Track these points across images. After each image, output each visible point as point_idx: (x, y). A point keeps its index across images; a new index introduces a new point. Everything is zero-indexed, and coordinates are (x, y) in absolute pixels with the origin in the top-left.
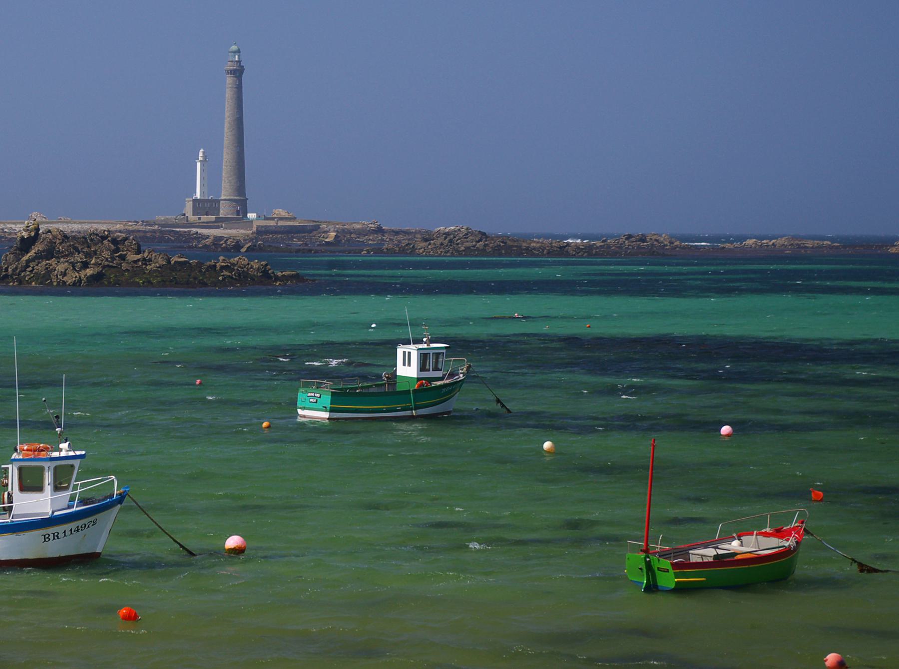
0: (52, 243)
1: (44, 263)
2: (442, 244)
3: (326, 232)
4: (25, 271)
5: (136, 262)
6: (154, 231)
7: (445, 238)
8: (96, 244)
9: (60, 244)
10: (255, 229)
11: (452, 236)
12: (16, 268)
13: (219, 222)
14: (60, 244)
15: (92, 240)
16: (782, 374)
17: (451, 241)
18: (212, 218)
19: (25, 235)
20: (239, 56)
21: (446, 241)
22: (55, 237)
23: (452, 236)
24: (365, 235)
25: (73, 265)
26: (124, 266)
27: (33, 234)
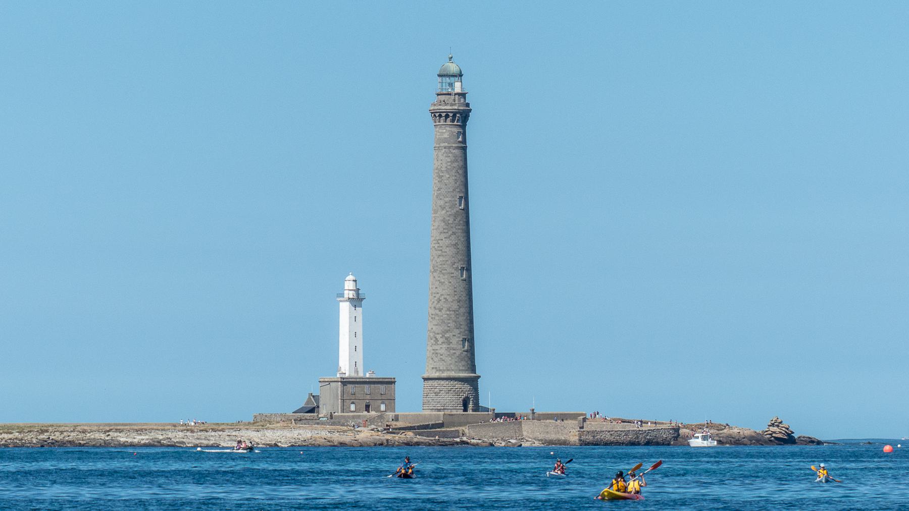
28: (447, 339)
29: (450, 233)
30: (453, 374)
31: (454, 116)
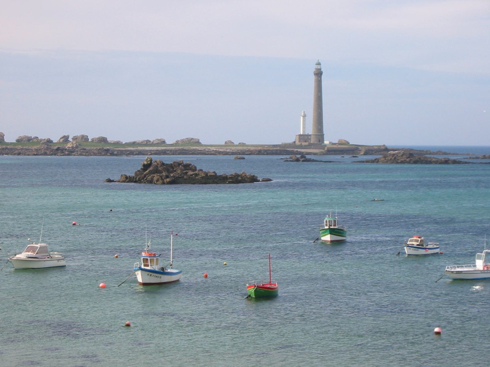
0: (157, 166)
1: (152, 176)
2: (391, 159)
3: (360, 150)
4: (143, 179)
5: (192, 175)
6: (277, 150)
7: (393, 156)
8: (176, 167)
9: (160, 167)
10: (326, 149)
11: (396, 156)
12: (140, 178)
13: (310, 146)
14: (160, 167)
15: (174, 165)
16: (138, 290)
17: (395, 158)
18: (307, 143)
19: (145, 163)
20: (320, 67)
21: (393, 158)
22: (158, 164)
23: (396, 156)
24: (379, 152)
25: (161, 177)
26: (185, 177)
27: (149, 162)
30: (317, 134)
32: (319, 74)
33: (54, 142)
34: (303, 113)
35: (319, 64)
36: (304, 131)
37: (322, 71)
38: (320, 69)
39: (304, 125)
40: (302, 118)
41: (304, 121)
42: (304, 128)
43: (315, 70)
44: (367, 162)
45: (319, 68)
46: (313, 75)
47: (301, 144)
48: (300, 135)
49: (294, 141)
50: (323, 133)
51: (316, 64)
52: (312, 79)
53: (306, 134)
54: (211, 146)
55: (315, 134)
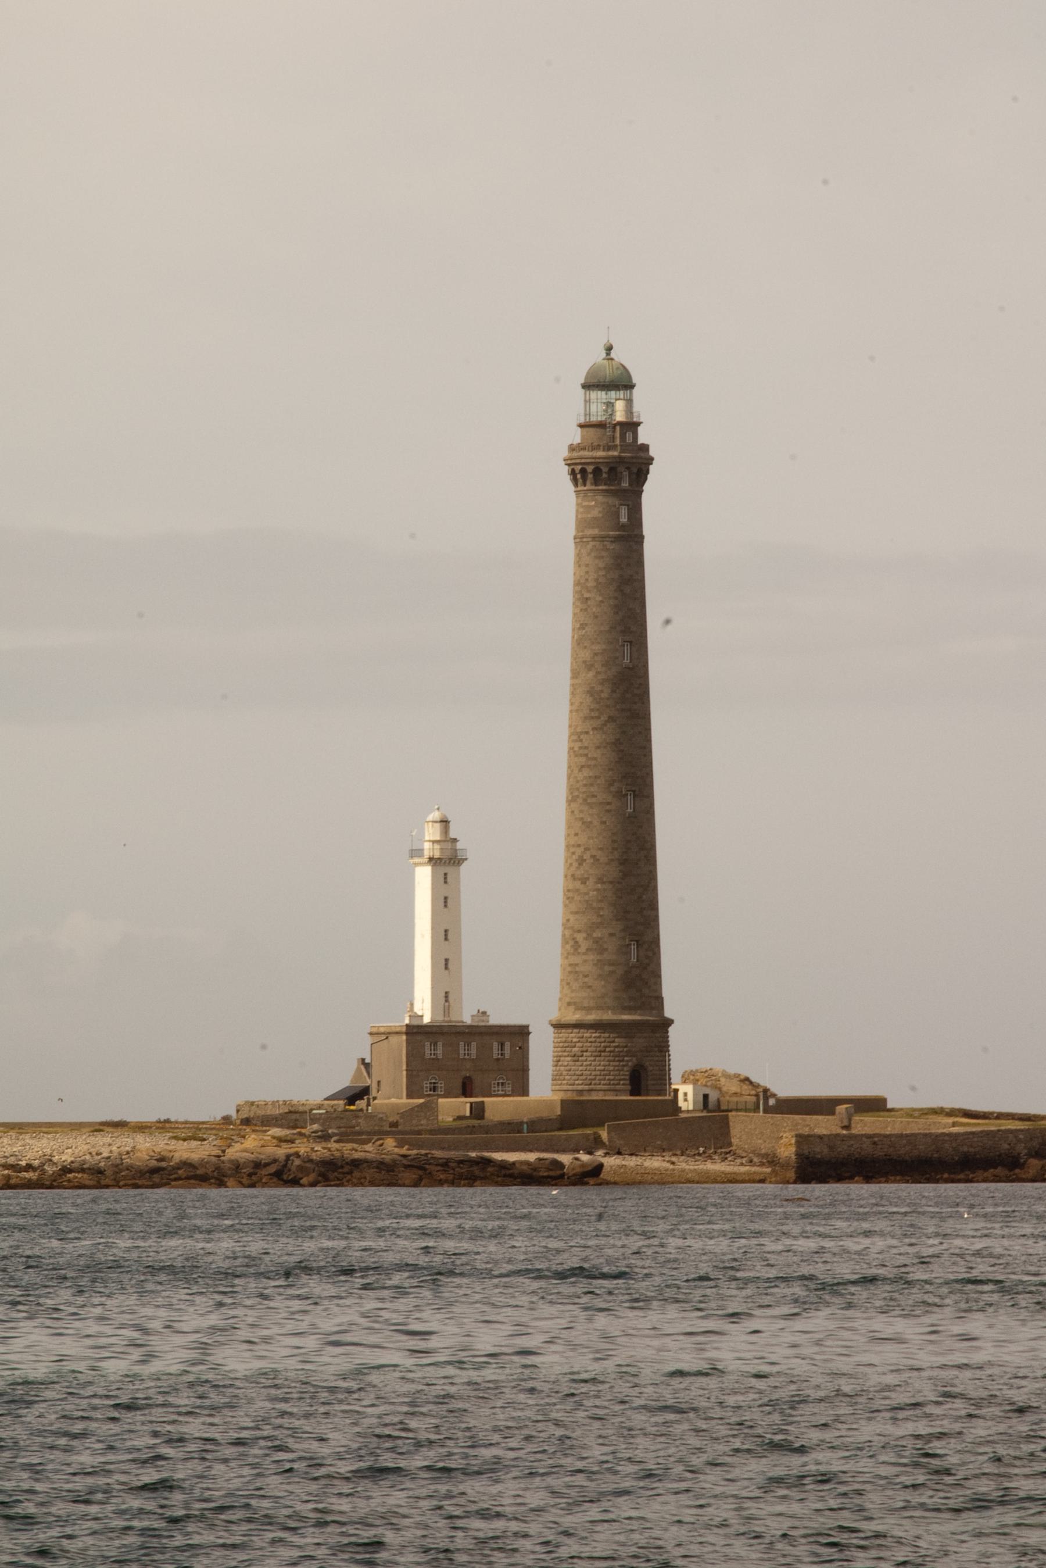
28: (596, 941)
29: (604, 718)
30: (608, 1016)
31: (612, 470)
32: (614, 470)
33: (889, 1106)
34: (432, 832)
35: (619, 382)
36: (444, 998)
37: (645, 448)
38: (631, 426)
39: (445, 935)
40: (424, 876)
41: (445, 902)
42: (445, 965)
43: (576, 437)
44: (773, 1345)
45: (620, 416)
46: (563, 473)
47: (478, 1111)
48: (416, 1032)
49: (344, 1079)
50: (658, 1001)
51: (587, 386)
52: (557, 512)
53: (468, 1020)
54: (1000, 1116)
55: (592, 1017)
